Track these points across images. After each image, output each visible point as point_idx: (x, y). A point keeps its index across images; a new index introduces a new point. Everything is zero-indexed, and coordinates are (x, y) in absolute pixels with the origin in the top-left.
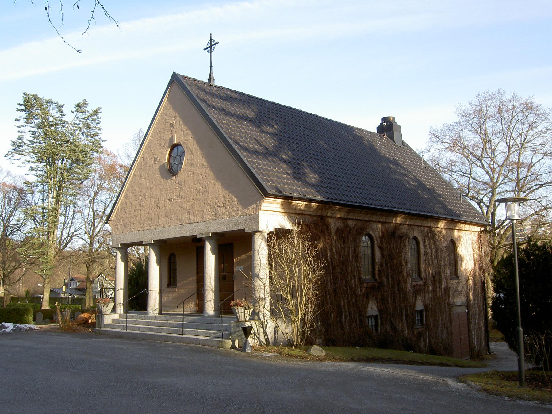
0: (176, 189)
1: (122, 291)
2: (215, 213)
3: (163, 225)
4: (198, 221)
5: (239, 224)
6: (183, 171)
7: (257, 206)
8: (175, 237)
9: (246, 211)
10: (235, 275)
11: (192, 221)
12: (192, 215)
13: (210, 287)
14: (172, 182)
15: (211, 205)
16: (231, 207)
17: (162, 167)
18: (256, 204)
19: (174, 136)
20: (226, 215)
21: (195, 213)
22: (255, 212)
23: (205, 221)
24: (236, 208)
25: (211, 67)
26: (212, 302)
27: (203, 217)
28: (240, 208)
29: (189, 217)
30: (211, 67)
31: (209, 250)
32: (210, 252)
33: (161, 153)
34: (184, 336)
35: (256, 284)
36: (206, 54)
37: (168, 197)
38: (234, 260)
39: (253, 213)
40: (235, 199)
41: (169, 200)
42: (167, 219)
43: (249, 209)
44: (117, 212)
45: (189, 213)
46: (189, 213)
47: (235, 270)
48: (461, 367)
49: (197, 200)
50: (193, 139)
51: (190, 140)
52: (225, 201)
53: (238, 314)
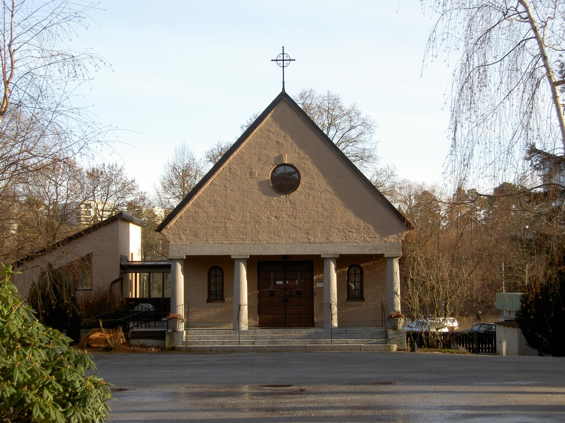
0: (286, 208)
1: (183, 305)
2: (345, 237)
3: (265, 241)
4: (320, 242)
5: (377, 249)
6: (298, 192)
7: (398, 236)
8: (286, 254)
9: (385, 239)
10: (315, 291)
11: (312, 241)
12: (311, 235)
13: (334, 302)
14: (280, 201)
15: (340, 229)
16: (366, 233)
17: (262, 185)
18: (397, 234)
19: (285, 156)
20: (360, 240)
21: (316, 234)
22: (396, 241)
23: (331, 242)
24: (373, 235)
25: (283, 82)
26: (336, 315)
27: (328, 239)
28: (378, 236)
29: (308, 237)
30: (283, 82)
31: (334, 269)
32: (334, 271)
33: (262, 170)
34: (332, 345)
35: (395, 300)
36: (276, 68)
37: (275, 214)
38: (315, 277)
39: (394, 241)
40: (372, 228)
41: (276, 217)
42: (272, 235)
43: (389, 238)
44: (179, 220)
45: (308, 234)
46: (308, 234)
47: (315, 286)
48: (386, 384)
49: (319, 223)
50: (312, 164)
51: (309, 164)
52: (359, 228)
53: (398, 324)
